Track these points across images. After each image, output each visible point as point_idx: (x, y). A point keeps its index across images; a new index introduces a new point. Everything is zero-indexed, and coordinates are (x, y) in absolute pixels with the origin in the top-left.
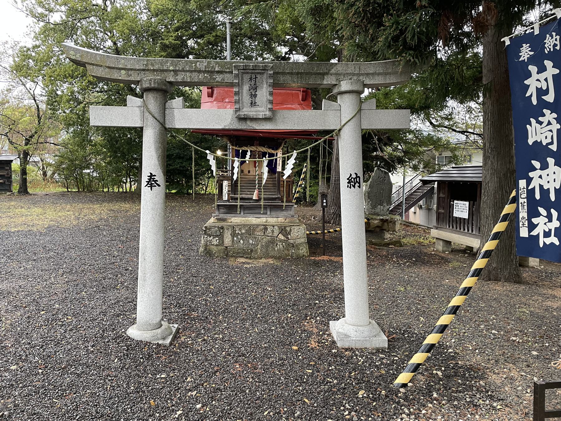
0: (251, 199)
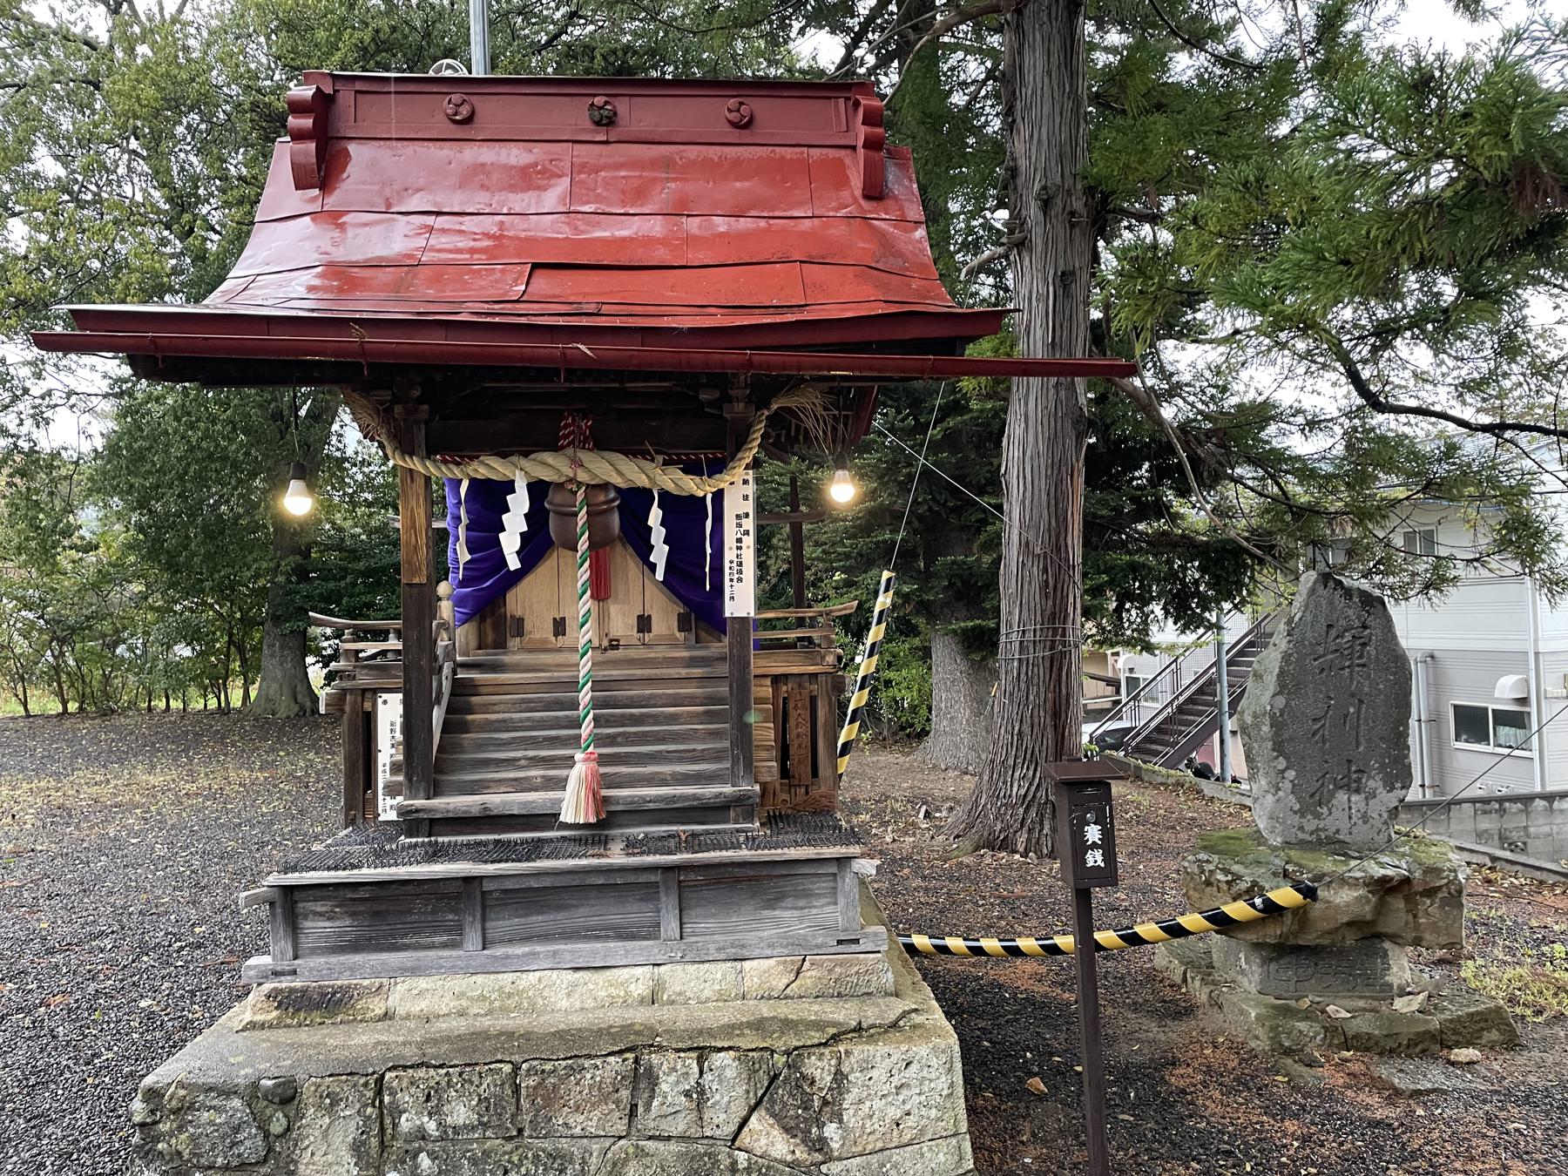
0: (550, 819)
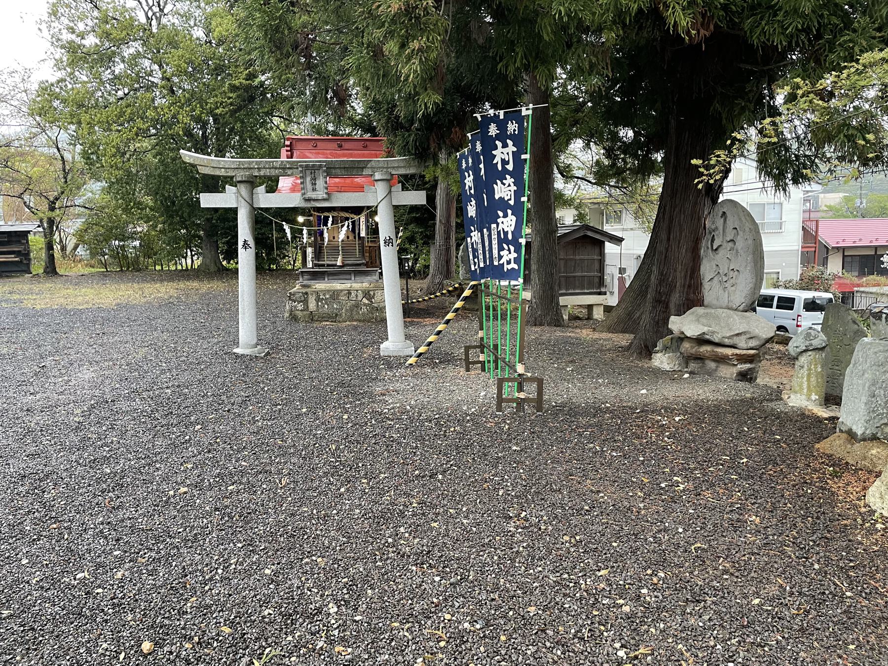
0: (336, 265)
